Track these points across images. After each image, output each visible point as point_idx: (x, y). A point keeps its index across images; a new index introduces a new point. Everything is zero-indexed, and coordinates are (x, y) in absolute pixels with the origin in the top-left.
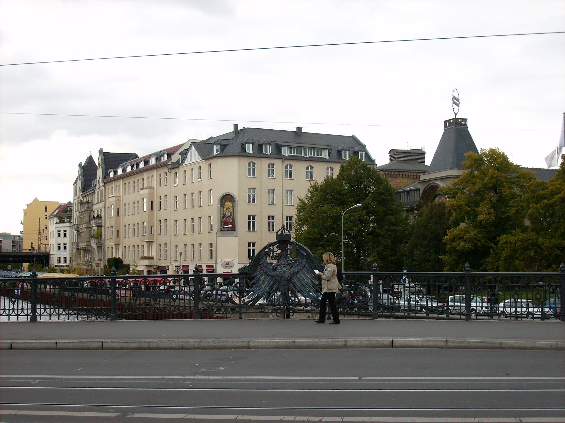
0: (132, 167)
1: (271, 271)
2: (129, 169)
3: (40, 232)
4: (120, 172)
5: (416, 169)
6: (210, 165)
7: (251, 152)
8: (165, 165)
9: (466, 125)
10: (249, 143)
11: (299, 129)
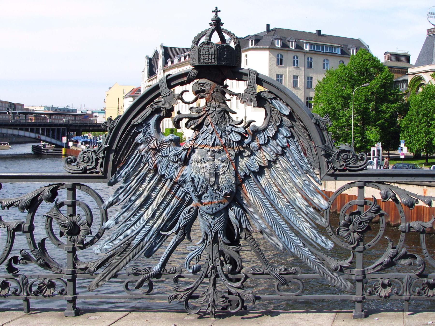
0: (185, 57)
2: (183, 59)
3: (118, 109)
4: (176, 61)
5: (403, 66)
11: (319, 32)
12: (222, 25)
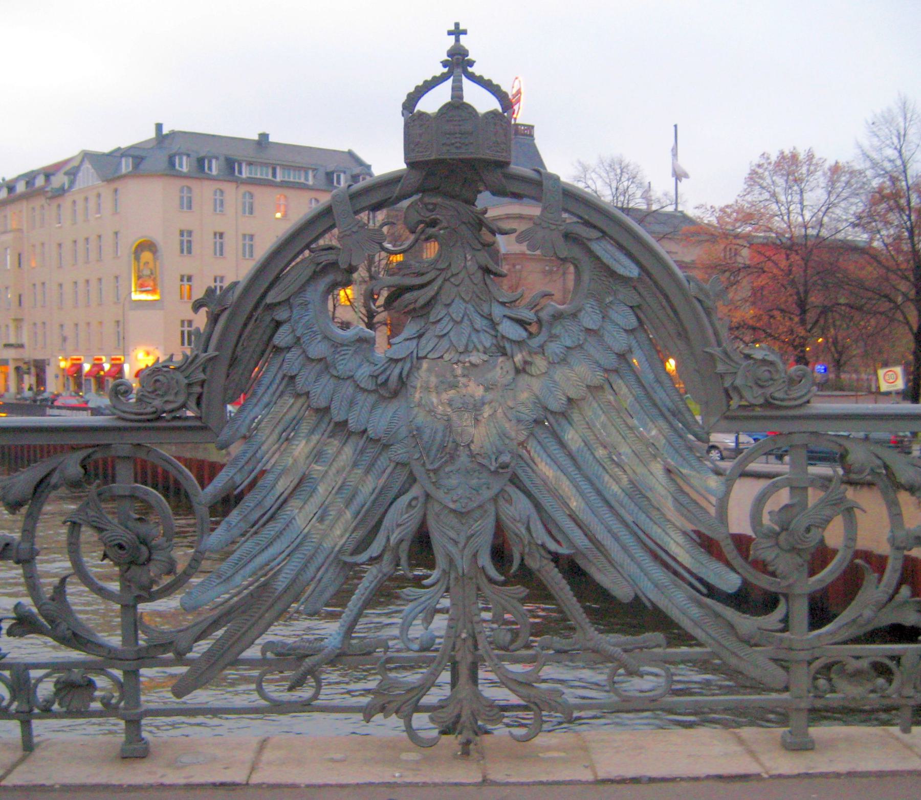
1: (361, 397)
6: (116, 191)
7: (185, 169)
8: (41, 192)
9: (531, 136)
10: (181, 154)
11: (264, 136)
12: (471, 66)
